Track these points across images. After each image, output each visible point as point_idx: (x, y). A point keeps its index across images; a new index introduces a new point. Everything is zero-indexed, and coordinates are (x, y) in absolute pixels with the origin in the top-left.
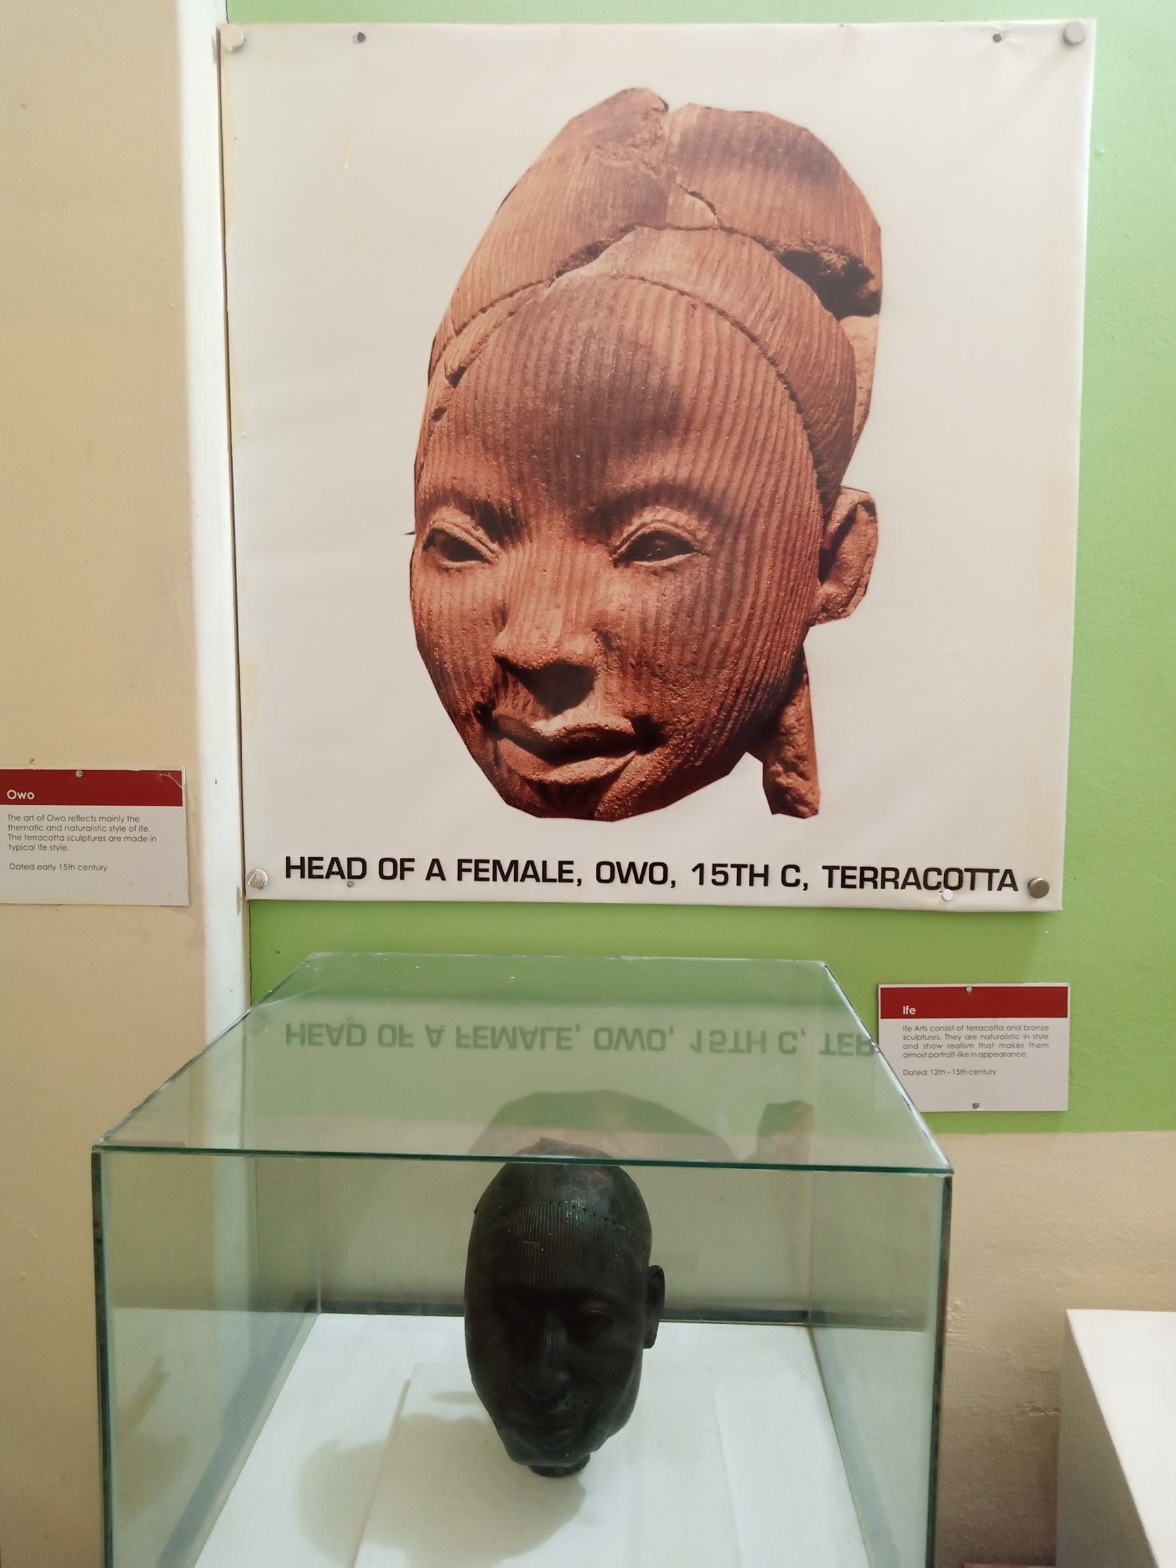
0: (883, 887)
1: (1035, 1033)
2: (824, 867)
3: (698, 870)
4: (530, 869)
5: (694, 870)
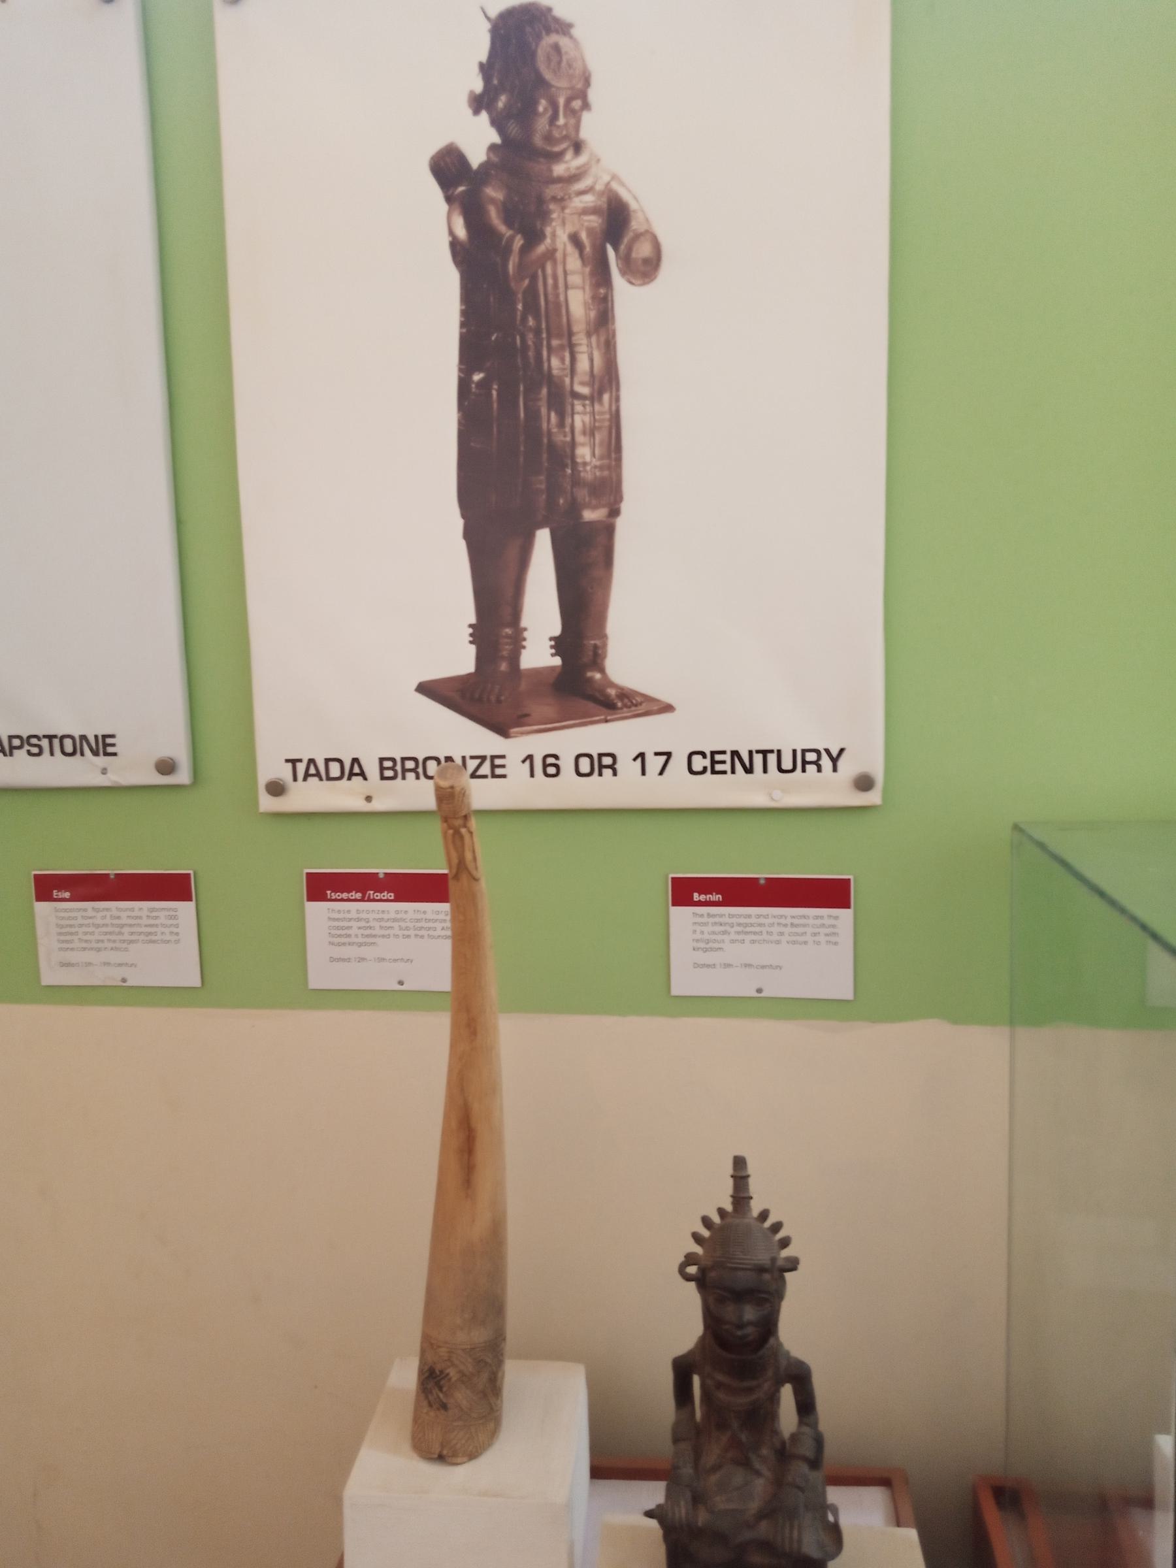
0: (11, 754)
1: (167, 913)
2: (287, 761)
3: (639, 760)
4: (356, 766)
5: (524, 761)
